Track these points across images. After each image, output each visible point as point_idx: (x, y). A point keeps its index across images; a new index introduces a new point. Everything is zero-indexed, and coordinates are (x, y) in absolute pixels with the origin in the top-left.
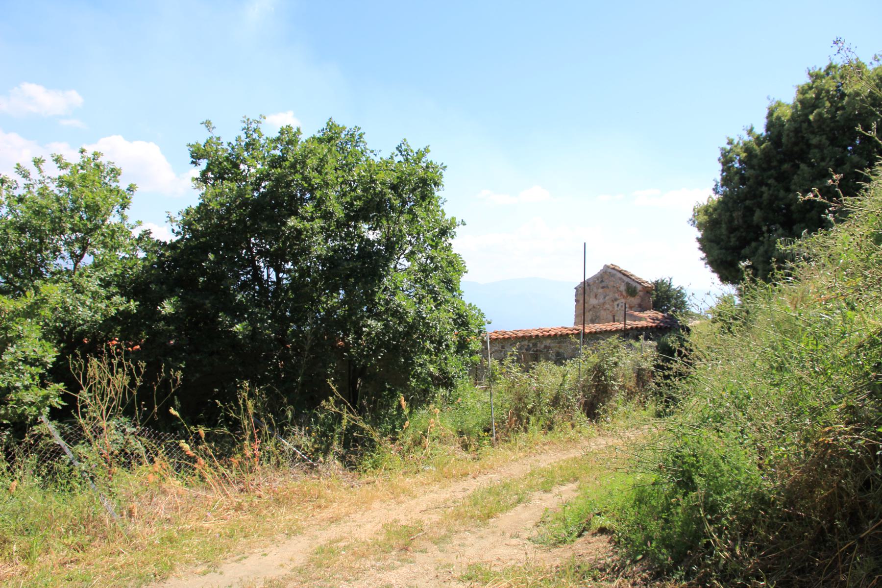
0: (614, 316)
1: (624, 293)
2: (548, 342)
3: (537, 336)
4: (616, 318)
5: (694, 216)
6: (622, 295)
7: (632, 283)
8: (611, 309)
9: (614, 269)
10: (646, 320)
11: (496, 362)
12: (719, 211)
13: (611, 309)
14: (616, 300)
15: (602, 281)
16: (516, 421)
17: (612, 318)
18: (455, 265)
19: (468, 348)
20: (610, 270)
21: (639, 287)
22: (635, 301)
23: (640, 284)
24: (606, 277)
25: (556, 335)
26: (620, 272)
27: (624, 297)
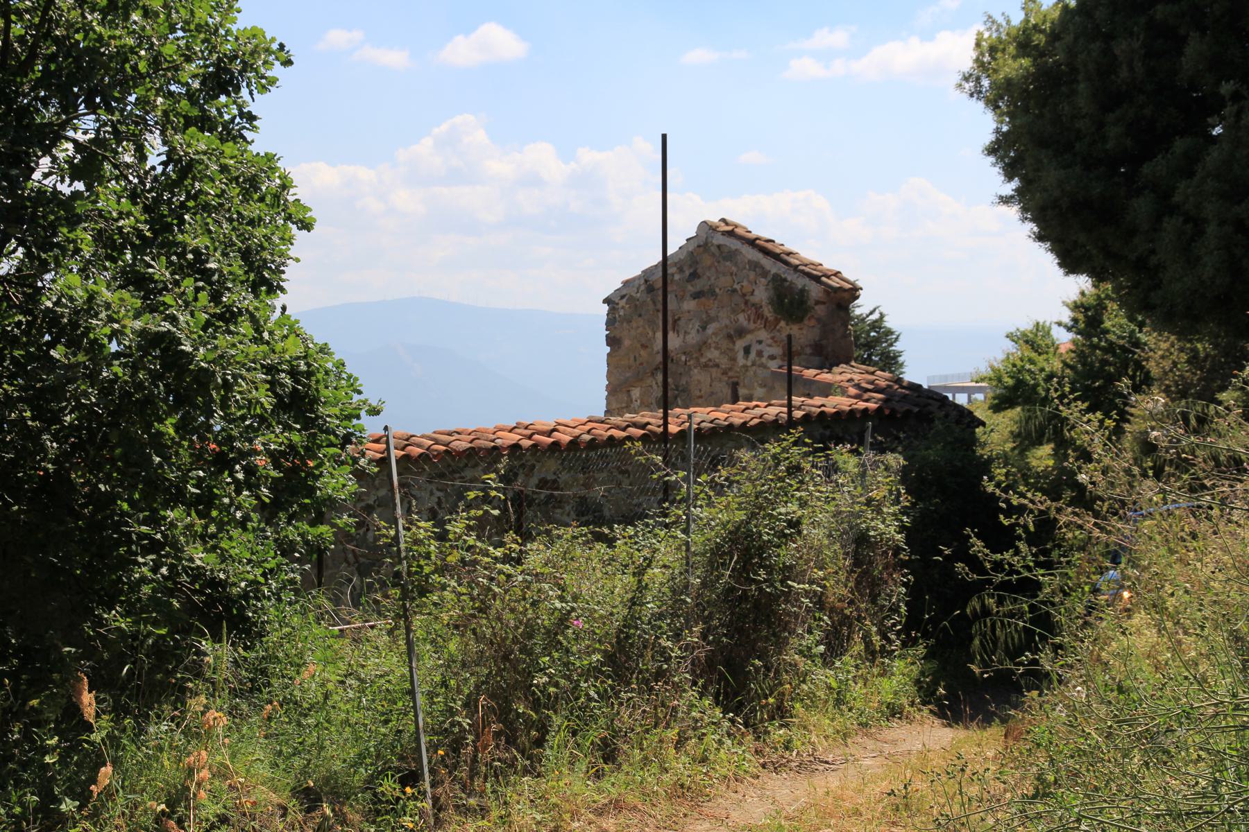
0: (734, 387)
1: (768, 312)
2: (549, 468)
3: (516, 447)
4: (742, 391)
5: (979, 62)
6: (759, 316)
7: (790, 276)
8: (724, 362)
9: (731, 234)
10: (844, 392)
11: (424, 527)
12: (1069, 38)
13: (724, 362)
14: (741, 332)
15: (694, 275)
16: (497, 735)
17: (727, 392)
18: (265, 203)
19: (311, 491)
20: (719, 240)
21: (815, 291)
22: (803, 334)
23: (817, 279)
24: (707, 260)
25: (575, 443)
26: (753, 242)
27: (767, 325)
